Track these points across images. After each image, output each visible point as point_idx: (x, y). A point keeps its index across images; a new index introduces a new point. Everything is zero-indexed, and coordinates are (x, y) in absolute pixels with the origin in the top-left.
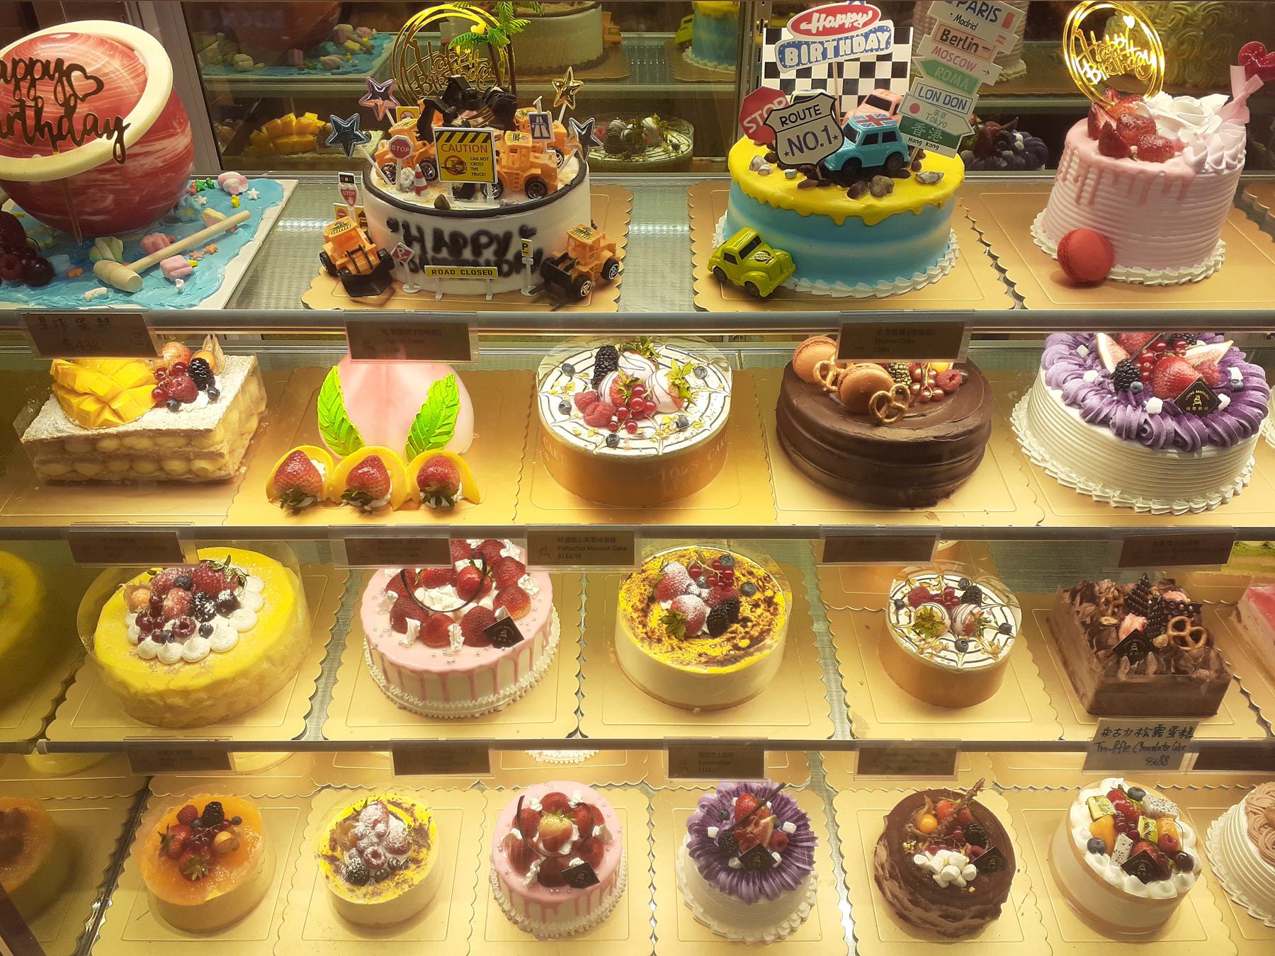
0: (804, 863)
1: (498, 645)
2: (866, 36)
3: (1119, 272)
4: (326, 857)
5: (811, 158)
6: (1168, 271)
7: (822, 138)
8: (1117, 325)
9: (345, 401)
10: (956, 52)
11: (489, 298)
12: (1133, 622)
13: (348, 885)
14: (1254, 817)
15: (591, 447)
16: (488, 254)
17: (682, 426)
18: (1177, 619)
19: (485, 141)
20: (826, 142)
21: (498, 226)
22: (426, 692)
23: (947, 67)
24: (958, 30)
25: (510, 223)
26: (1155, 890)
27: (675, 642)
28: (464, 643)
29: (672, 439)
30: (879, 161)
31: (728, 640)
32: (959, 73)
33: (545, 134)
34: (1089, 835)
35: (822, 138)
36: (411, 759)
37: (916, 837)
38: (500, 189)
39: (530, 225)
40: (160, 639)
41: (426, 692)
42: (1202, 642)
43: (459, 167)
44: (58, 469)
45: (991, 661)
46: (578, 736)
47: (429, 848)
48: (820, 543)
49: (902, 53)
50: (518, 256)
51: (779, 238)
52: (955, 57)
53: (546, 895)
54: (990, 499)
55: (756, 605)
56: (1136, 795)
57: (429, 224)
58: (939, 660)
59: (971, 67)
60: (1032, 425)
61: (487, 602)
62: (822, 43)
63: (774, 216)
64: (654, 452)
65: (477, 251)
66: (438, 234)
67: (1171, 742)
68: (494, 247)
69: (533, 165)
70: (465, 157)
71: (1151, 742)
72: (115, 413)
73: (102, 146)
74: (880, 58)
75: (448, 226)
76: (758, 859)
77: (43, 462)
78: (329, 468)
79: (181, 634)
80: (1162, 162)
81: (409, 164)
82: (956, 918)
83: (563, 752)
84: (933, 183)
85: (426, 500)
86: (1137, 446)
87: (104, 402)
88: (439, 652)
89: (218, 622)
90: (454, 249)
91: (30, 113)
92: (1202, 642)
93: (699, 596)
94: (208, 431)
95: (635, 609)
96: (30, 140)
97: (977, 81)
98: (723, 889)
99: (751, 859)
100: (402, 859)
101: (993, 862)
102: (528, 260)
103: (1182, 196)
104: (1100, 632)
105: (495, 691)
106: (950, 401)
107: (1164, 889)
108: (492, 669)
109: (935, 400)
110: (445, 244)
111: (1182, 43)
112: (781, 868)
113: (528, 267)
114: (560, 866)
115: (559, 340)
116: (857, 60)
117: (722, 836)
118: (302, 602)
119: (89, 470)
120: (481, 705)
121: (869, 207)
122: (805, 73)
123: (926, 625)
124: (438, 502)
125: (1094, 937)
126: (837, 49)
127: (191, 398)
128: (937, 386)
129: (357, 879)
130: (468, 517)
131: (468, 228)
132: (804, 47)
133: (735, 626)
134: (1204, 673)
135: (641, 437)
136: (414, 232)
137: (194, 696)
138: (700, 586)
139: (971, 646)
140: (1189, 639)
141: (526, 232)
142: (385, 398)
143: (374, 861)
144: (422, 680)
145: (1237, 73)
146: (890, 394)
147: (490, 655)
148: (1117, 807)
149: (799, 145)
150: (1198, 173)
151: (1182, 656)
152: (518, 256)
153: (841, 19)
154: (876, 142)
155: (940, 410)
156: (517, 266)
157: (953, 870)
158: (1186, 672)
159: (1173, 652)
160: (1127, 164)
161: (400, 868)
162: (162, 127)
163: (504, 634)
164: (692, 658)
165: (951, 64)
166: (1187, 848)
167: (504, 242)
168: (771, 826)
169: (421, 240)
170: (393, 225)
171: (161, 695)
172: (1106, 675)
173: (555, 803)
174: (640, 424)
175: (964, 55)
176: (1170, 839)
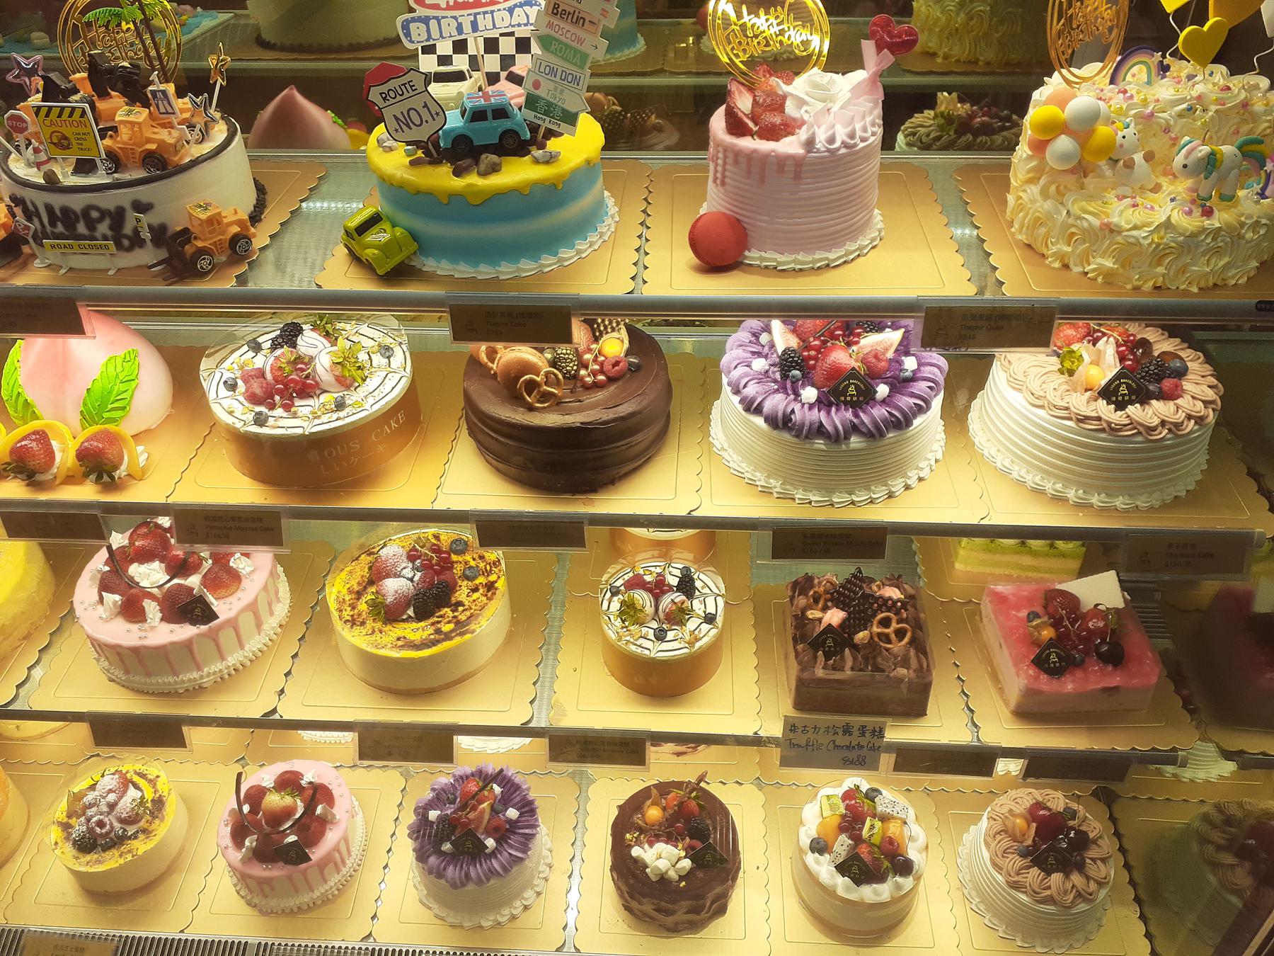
0: (517, 849)
1: (194, 622)
3: (753, 256)
4: (60, 824)
7: (426, 116)
8: (789, 311)
10: (567, 27)
11: (111, 273)
12: (835, 616)
13: (74, 852)
14: (992, 822)
15: (239, 425)
16: (103, 228)
18: (883, 615)
19: (82, 116)
20: (430, 119)
21: (109, 201)
22: (130, 664)
23: (560, 42)
25: (122, 198)
26: (868, 893)
27: (378, 625)
28: (162, 620)
29: (325, 418)
30: (496, 136)
31: (433, 624)
32: (572, 48)
33: (170, 110)
34: (814, 834)
35: (426, 116)
36: (111, 731)
37: (641, 830)
41: (130, 664)
42: (906, 640)
43: (65, 143)
45: (686, 651)
46: (277, 716)
47: (162, 820)
48: (767, 535)
50: (136, 232)
51: (402, 217)
53: (259, 871)
54: (671, 487)
55: (475, 590)
56: (872, 795)
57: (40, 199)
58: (633, 648)
59: (581, 41)
60: (981, 418)
61: (194, 581)
62: (455, 18)
63: (395, 191)
64: (300, 431)
65: (91, 225)
67: (864, 741)
68: (107, 222)
69: (149, 141)
70: (68, 132)
71: (841, 740)
75: (57, 201)
76: (469, 844)
80: (777, 140)
82: (668, 913)
83: (327, 733)
84: (547, 162)
85: (86, 476)
86: (786, 436)
88: (135, 627)
90: (68, 224)
92: (906, 640)
93: (411, 580)
95: (350, 591)
97: (587, 56)
99: (472, 841)
100: (131, 830)
101: (708, 857)
102: (146, 235)
103: (798, 176)
104: (805, 625)
106: (612, 388)
107: (876, 893)
108: (188, 645)
109: (597, 386)
110: (59, 219)
111: (971, 19)
112: (494, 854)
113: (148, 242)
114: (282, 839)
115: (250, 315)
116: (512, 34)
117: (441, 819)
118: (50, 578)
120: (183, 682)
121: (470, 185)
122: (429, 50)
123: (629, 612)
124: (99, 478)
125: (820, 937)
128: (602, 371)
129: (87, 844)
130: (137, 494)
131: (77, 202)
132: (433, 23)
133: (447, 611)
134: (902, 671)
135: (295, 416)
138: (414, 569)
139: (670, 635)
140: (893, 636)
142: (62, 371)
143: (98, 830)
145: (868, 47)
146: (538, 379)
147: (185, 632)
148: (847, 808)
150: (809, 152)
151: (880, 653)
152: (136, 232)
154: (486, 119)
155: (600, 395)
156: (136, 242)
157: (663, 865)
158: (883, 671)
159: (870, 654)
160: (747, 143)
161: (130, 838)
163: (198, 611)
164: (388, 642)
165: (562, 38)
166: (912, 854)
167: (117, 217)
168: (488, 811)
172: (802, 670)
173: (288, 782)
174: (298, 402)
175: (573, 29)
176: (891, 841)
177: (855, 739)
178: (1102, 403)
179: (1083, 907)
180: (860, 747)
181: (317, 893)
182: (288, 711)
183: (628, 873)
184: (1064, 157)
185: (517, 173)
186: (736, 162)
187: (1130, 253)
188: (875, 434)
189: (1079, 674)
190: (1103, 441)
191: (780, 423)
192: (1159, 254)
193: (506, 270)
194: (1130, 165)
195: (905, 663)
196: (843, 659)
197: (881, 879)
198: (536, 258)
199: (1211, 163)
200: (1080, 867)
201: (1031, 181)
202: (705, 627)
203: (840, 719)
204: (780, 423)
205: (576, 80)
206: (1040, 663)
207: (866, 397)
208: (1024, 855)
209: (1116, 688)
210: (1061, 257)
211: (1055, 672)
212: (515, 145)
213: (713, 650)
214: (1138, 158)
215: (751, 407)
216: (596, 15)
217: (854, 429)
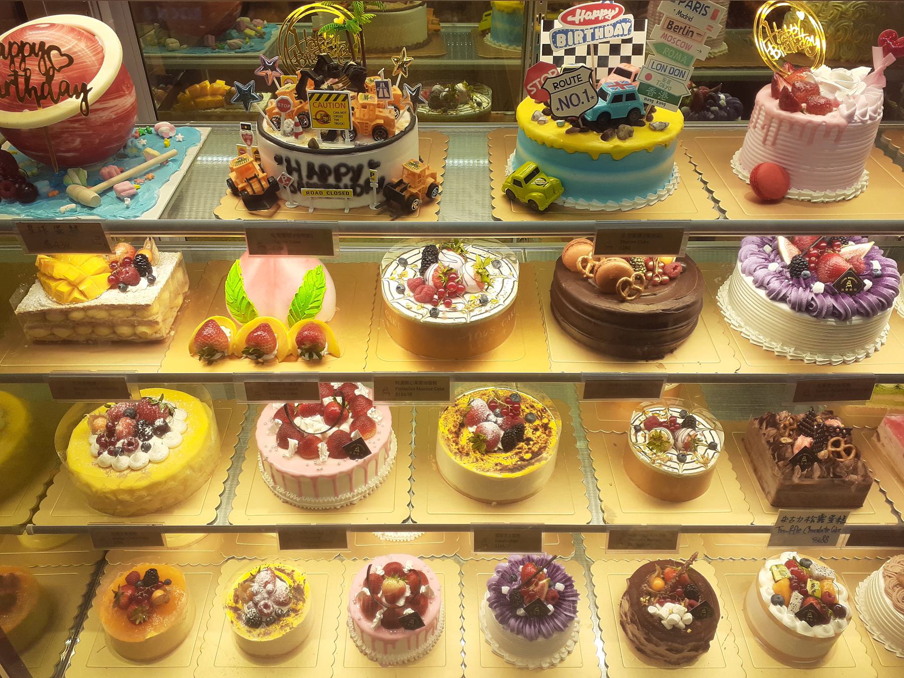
0: (570, 612)
1: (353, 457)
2: (614, 25)
3: (793, 193)
4: (231, 608)
5: (575, 112)
6: (828, 192)
7: (583, 98)
8: (792, 231)
9: (245, 284)
10: (678, 37)
11: (346, 211)
12: (804, 441)
13: (246, 628)
14: (889, 579)
15: (419, 317)
16: (346, 180)
17: (484, 302)
18: (834, 439)
19: (344, 100)
20: (586, 101)
21: (353, 161)
22: (302, 491)
23: (671, 48)
24: (679, 21)
25: (362, 158)
26: (819, 631)
27: (478, 455)
28: (329, 456)
29: (477, 311)
30: (623, 114)
31: (516, 454)
32: (680, 52)
33: (387, 95)
34: (772, 592)
35: (583, 98)
36: (291, 538)
37: (650, 594)
38: (355, 134)
39: (376, 159)
40: (113, 453)
41: (302, 491)
42: (852, 455)
43: (326, 119)
44: (41, 333)
45: (702, 469)
46: (410, 522)
47: (304, 601)
48: (581, 385)
49: (640, 37)
50: (368, 182)
51: (552, 169)
52: (677, 40)
53: (387, 635)
54: (702, 354)
55: (536, 429)
56: (805, 564)
57: (304, 159)
58: (666, 468)
59: (689, 47)
60: (732, 301)
61: (345, 427)
62: (583, 30)
63: (549, 153)
64: (463, 321)
65: (338, 178)
66: (310, 166)
67: (830, 526)
68: (350, 175)
69: (378, 117)
70: (330, 111)
71: (816, 526)
72: (82, 293)
73: (72, 103)
74: (624, 41)
75: (317, 160)
76: (537, 609)
77: (31, 328)
78: (233, 332)
79: (128, 449)
80: (824, 115)
81: (290, 116)
82: (678, 651)
83: (399, 533)
84: (662, 130)
85: (302, 354)
86: (806, 316)
87: (74, 285)
88: (311, 462)
89: (154, 441)
90: (322, 177)
91: (21, 80)
92: (852, 455)
93: (496, 422)
94: (148, 306)
95: (450, 432)
96: (21, 99)
97: (692, 57)
98: (512, 630)
99: (532, 609)
100: (285, 609)
101: (704, 611)
102: (375, 185)
103: (838, 139)
104: (780, 448)
105: (351, 490)
106: (674, 284)
107: (825, 631)
108: (349, 475)
109: (663, 283)
110: (316, 173)
111: (838, 31)
112: (554, 616)
113: (375, 190)
114: (397, 614)
115: (397, 241)
116: (608, 42)
117: (512, 593)
118: (214, 427)
119: (63, 333)
120: (341, 500)
121: (616, 147)
122: (570, 52)
123: (656, 443)
124: (311, 356)
125: (776, 664)
126: (593, 35)
127: (135, 282)
128: (664, 274)
129: (253, 623)
130: (332, 366)
131: (332, 162)
132: (570, 34)
133: (521, 444)
134: (853, 477)
135: (455, 310)
136: (294, 165)
137: (137, 494)
138: (497, 416)
139: (689, 458)
140: (843, 453)
141: (373, 165)
142: (273, 282)
143: (265, 611)
144: (299, 482)
145: (877, 52)
146: (631, 280)
147: (347, 464)
148: (792, 572)
149: (567, 103)
150: (849, 122)
151: (838, 465)
152: (368, 182)
153: (596, 14)
154: (621, 101)
155: (666, 290)
156: (367, 188)
157: (676, 617)
158: (841, 477)
159: (831, 463)
160: (799, 116)
161: (284, 616)
162: (115, 90)
163: (357, 450)
164: (491, 467)
165: (674, 45)
166: (842, 602)
167: (357, 172)
168: (547, 586)
169: (299, 170)
170: (278, 160)
171: (114, 493)
172: (784, 479)
173: (394, 570)
174: (454, 301)
175: (683, 39)
176: (829, 595)
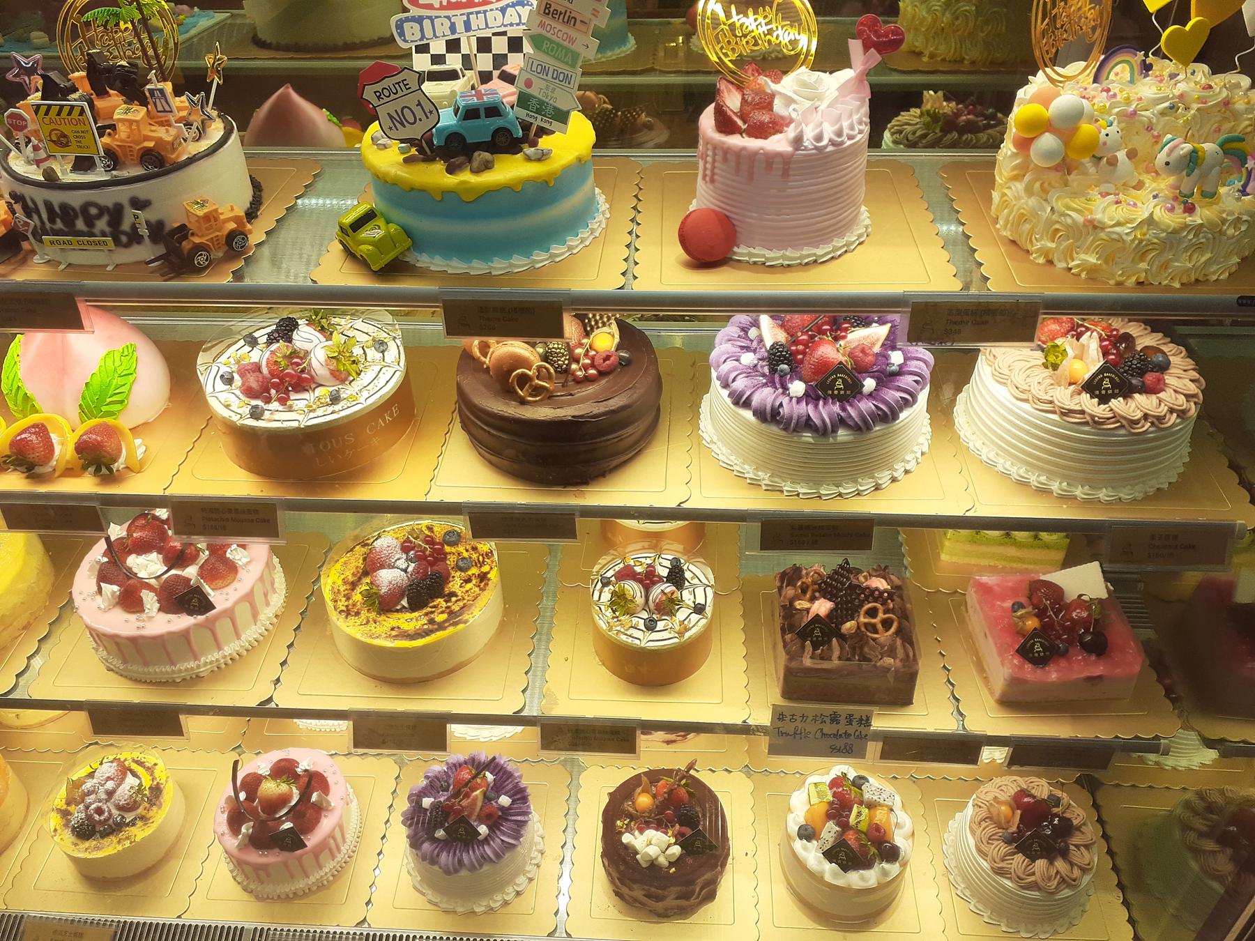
0: (509, 836)
1: (191, 613)
3: (742, 252)
4: (59, 811)
7: (419, 114)
8: (778, 306)
10: (559, 27)
11: (109, 268)
12: (822, 607)
13: (73, 839)
14: (977, 809)
15: (235, 418)
16: (102, 224)
18: (870, 605)
19: (81, 114)
20: (423, 117)
21: (107, 198)
22: (128, 654)
23: (552, 41)
25: (120, 195)
26: (855, 879)
27: (373, 615)
28: (159, 610)
29: (320, 412)
30: (489, 134)
31: (426, 614)
32: (563, 47)
33: (167, 108)
34: (802, 821)
35: (419, 114)
36: (109, 720)
37: (632, 817)
41: (128, 654)
42: (893, 630)
43: (64, 140)
45: (676, 640)
46: (272, 705)
47: (160, 807)
48: (756, 527)
50: (134, 228)
51: (396, 214)
53: (256, 857)
54: (661, 479)
55: (468, 581)
56: (859, 782)
57: (39, 196)
58: (624, 638)
59: (572, 41)
60: (966, 411)
61: (191, 572)
62: (448, 18)
63: (389, 188)
64: (295, 424)
65: (90, 222)
67: (851, 730)
68: (105, 219)
69: (147, 138)
70: (67, 130)
71: (829, 728)
75: (57, 197)
76: (462, 831)
80: (766, 138)
82: (658, 899)
83: (322, 722)
84: (539, 160)
85: (84, 468)
86: (774, 429)
88: (133, 617)
90: (67, 221)
92: (893, 630)
93: (405, 571)
95: (345, 582)
97: (578, 55)
99: (465, 828)
100: (129, 817)
101: (698, 844)
102: (144, 231)
103: (786, 173)
104: (793, 615)
106: (603, 382)
107: (863, 879)
108: (185, 635)
109: (588, 380)
110: (58, 216)
111: (957, 19)
112: (486, 840)
113: (146, 238)
114: (277, 826)
115: (246, 310)
116: (504, 33)
117: (435, 806)
118: (49, 569)
120: (180, 671)
121: (463, 182)
122: (423, 49)
123: (620, 602)
124: (98, 470)
125: (807, 923)
128: (593, 366)
129: (85, 831)
130: (135, 486)
131: (76, 199)
132: (427, 23)
133: (440, 601)
134: (889, 661)
135: (290, 409)
138: (408, 560)
139: (660, 625)
140: (879, 626)
142: (61, 365)
143: (97, 817)
145: (855, 46)
146: (530, 373)
147: (182, 622)
148: (834, 795)
150: (797, 149)
151: (867, 642)
152: (134, 228)
154: (479, 117)
155: (591, 389)
156: (134, 238)
157: (653, 851)
158: (870, 660)
159: (857, 643)
160: (736, 141)
161: (128, 825)
163: (195, 602)
164: (382, 632)
165: (554, 38)
166: (899, 841)
167: (116, 214)
168: (481, 798)
172: (790, 660)
173: (284, 770)
174: (293, 396)
175: (565, 29)
176: (878, 828)
177: (842, 727)
178: (1085, 397)
179: (1066, 893)
180: (847, 735)
181: (312, 879)
182: (283, 700)
183: (618, 859)
184: (1048, 155)
185: (510, 170)
186: (725, 159)
187: (1113, 249)
188: (862, 427)
189: (1063, 663)
190: (1087, 434)
191: (769, 416)
192: (1142, 250)
193: (498, 266)
194: (1113, 162)
195: (892, 652)
196: (830, 648)
197: (868, 865)
198: (528, 254)
199: (1192, 161)
200: (1064, 854)
201: (1016, 178)
202: (695, 617)
203: (828, 708)
204: (769, 416)
205: (567, 79)
206: (1025, 652)
207: (853, 390)
208: (1008, 841)
209: (1099, 677)
210: (1046, 253)
211: (1039, 662)
212: (508, 142)
213: (703, 640)
214: (1121, 155)
215: (740, 400)
216: (587, 15)
217: (841, 422)
